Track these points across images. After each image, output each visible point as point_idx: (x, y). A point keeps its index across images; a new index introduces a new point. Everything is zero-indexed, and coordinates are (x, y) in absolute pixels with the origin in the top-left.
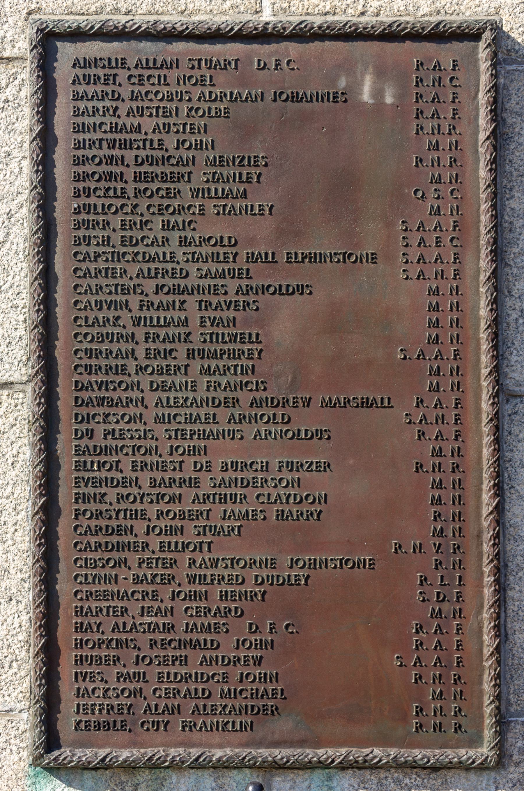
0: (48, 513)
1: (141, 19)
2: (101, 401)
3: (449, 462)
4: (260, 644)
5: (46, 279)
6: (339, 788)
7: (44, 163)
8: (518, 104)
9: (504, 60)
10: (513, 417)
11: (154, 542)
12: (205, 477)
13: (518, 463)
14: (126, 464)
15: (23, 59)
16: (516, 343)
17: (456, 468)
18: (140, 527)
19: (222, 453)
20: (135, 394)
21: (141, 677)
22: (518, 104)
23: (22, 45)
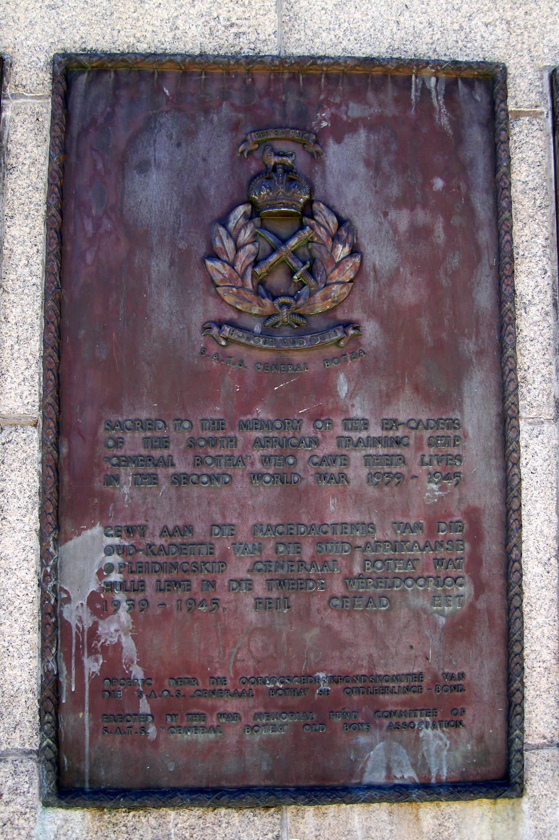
6: (268, 3)
8: (23, 135)
9: (12, 95)
10: (6, 445)
13: (10, 494)
15: (536, 115)
16: (11, 370)
22: (23, 135)
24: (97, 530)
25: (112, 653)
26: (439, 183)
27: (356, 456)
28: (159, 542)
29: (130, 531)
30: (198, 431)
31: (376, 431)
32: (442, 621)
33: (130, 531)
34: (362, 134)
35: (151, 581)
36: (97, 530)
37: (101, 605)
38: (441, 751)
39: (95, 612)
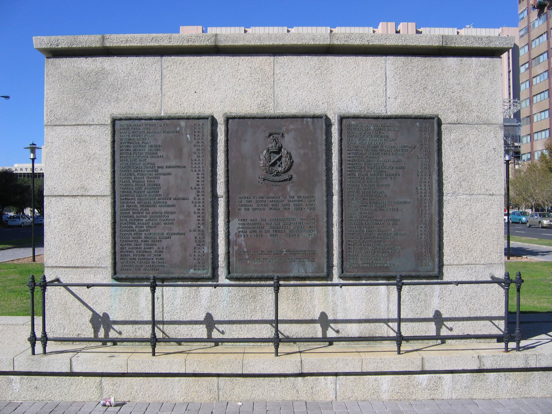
0: (114, 223)
1: (135, 116)
2: (126, 199)
3: (201, 212)
4: (160, 252)
5: (114, 172)
7: (113, 147)
11: (137, 230)
12: (148, 215)
14: (131, 213)
17: (203, 213)
18: (134, 226)
19: (151, 210)
20: (133, 197)
21: (134, 259)
23: (109, 122)
24: (237, 220)
25: (240, 246)
26: (310, 143)
27: (291, 204)
28: (250, 222)
29: (244, 220)
30: (258, 199)
31: (296, 198)
32: (310, 239)
33: (244, 220)
34: (293, 132)
35: (248, 231)
36: (237, 220)
37: (238, 235)
38: (309, 269)
39: (236, 237)
